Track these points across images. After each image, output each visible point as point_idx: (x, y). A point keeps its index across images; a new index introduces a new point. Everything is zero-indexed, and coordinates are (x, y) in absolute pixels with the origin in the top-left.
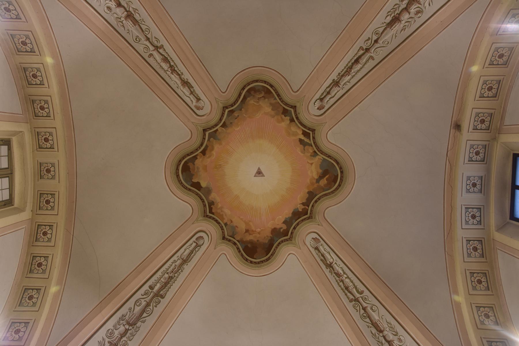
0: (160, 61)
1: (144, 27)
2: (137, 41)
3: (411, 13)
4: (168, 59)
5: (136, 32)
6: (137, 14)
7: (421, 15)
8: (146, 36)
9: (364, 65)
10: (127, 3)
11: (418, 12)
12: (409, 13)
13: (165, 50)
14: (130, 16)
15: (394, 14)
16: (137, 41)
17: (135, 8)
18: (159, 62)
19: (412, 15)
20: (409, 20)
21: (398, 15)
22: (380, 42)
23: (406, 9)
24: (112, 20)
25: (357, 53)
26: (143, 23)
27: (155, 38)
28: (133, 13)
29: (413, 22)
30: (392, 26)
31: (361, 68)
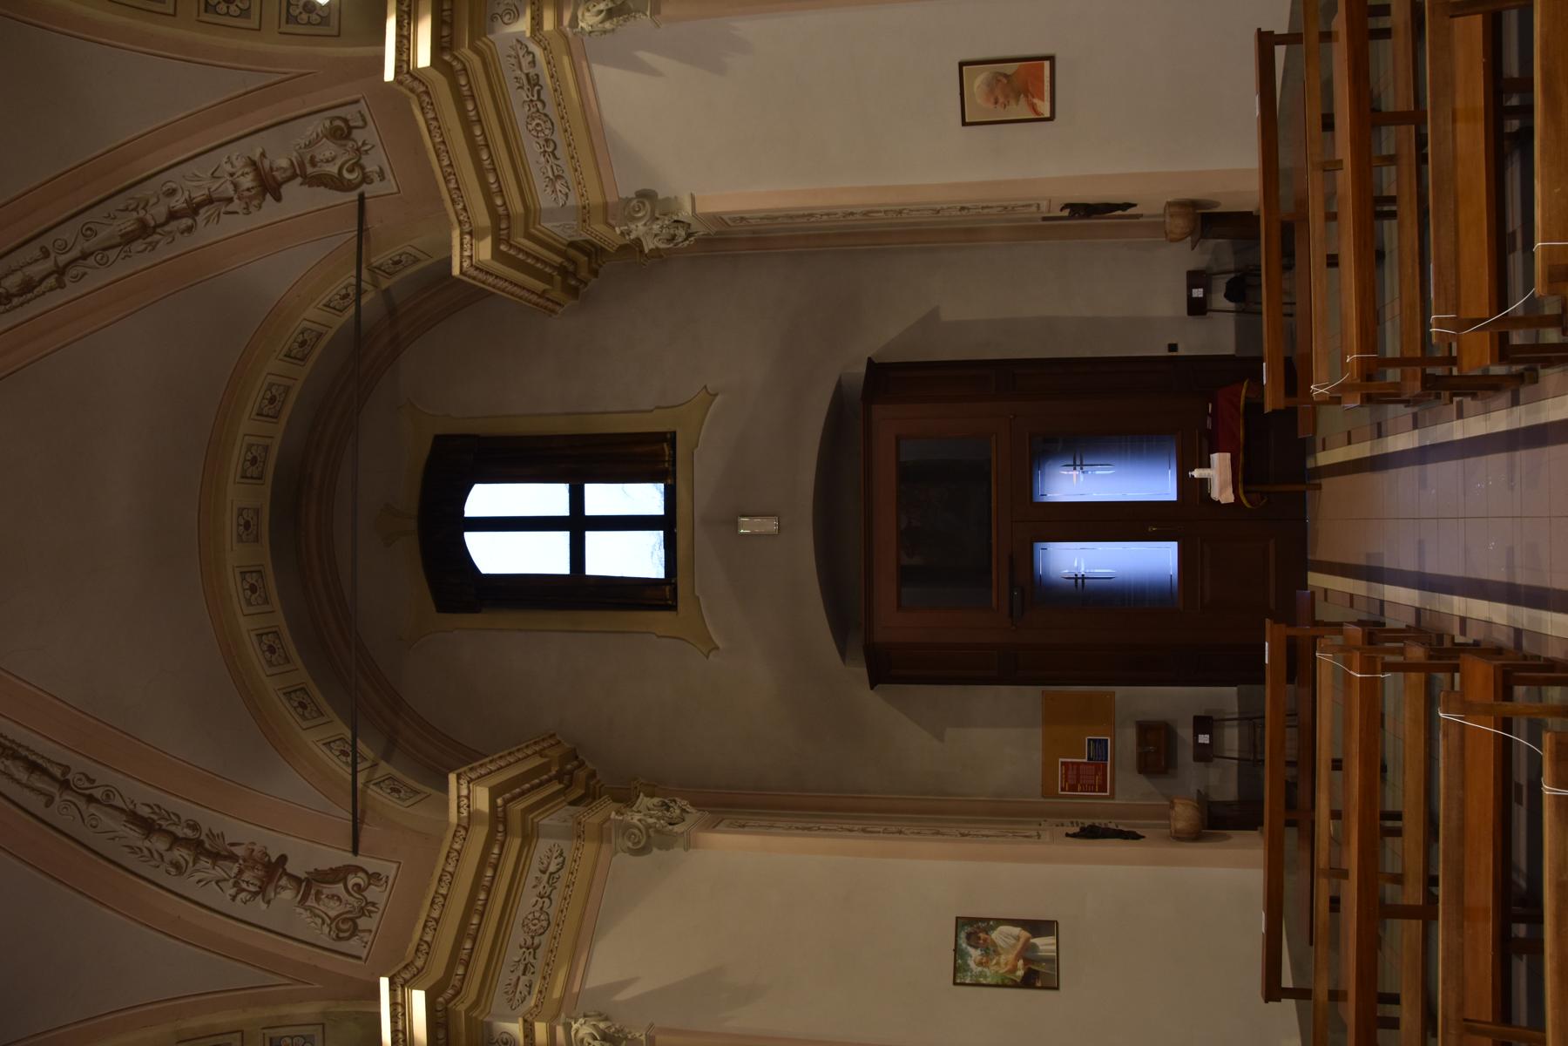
0: (27, 274)
1: (113, 254)
2: (87, 230)
3: (169, 852)
4: (29, 292)
5: (105, 233)
6: (144, 246)
7: (172, 873)
8: (92, 253)
9: (27, 787)
10: (171, 232)
11: (176, 865)
12: (170, 849)
13: (52, 289)
14: (144, 230)
15: (159, 819)
16: (87, 230)
17: (158, 246)
18: (25, 270)
19: (168, 856)
20: (156, 855)
21: (157, 827)
22: (93, 809)
23: (176, 841)
24: (147, 190)
25: (53, 762)
26: (122, 255)
27: (84, 274)
28: (149, 240)
29: (153, 863)
30: (132, 823)
31: (18, 782)
